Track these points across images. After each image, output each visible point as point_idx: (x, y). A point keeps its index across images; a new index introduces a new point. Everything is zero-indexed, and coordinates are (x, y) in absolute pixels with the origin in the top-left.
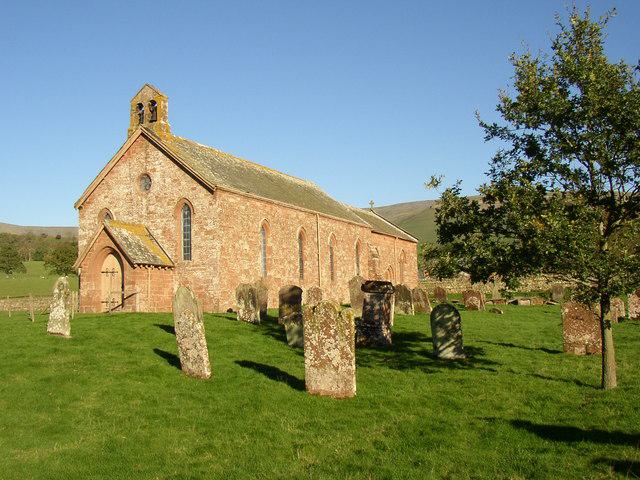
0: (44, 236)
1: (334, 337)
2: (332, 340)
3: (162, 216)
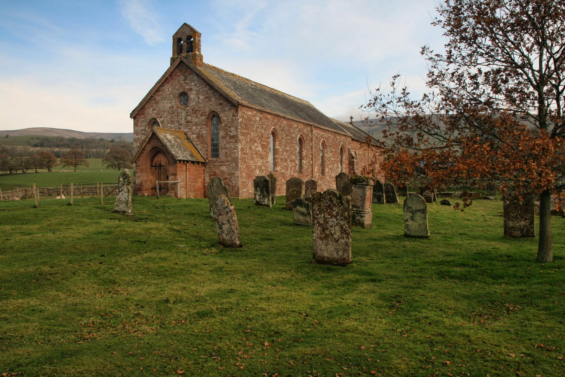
0: (102, 140)
1: (336, 217)
2: (334, 220)
3: (196, 124)
